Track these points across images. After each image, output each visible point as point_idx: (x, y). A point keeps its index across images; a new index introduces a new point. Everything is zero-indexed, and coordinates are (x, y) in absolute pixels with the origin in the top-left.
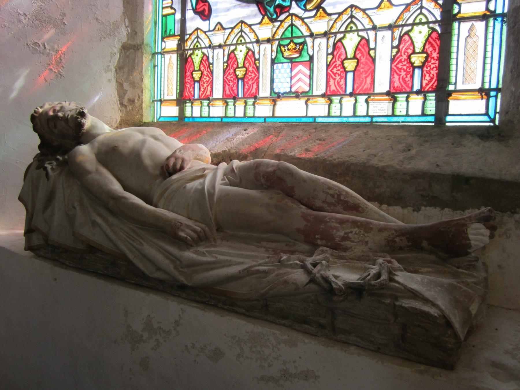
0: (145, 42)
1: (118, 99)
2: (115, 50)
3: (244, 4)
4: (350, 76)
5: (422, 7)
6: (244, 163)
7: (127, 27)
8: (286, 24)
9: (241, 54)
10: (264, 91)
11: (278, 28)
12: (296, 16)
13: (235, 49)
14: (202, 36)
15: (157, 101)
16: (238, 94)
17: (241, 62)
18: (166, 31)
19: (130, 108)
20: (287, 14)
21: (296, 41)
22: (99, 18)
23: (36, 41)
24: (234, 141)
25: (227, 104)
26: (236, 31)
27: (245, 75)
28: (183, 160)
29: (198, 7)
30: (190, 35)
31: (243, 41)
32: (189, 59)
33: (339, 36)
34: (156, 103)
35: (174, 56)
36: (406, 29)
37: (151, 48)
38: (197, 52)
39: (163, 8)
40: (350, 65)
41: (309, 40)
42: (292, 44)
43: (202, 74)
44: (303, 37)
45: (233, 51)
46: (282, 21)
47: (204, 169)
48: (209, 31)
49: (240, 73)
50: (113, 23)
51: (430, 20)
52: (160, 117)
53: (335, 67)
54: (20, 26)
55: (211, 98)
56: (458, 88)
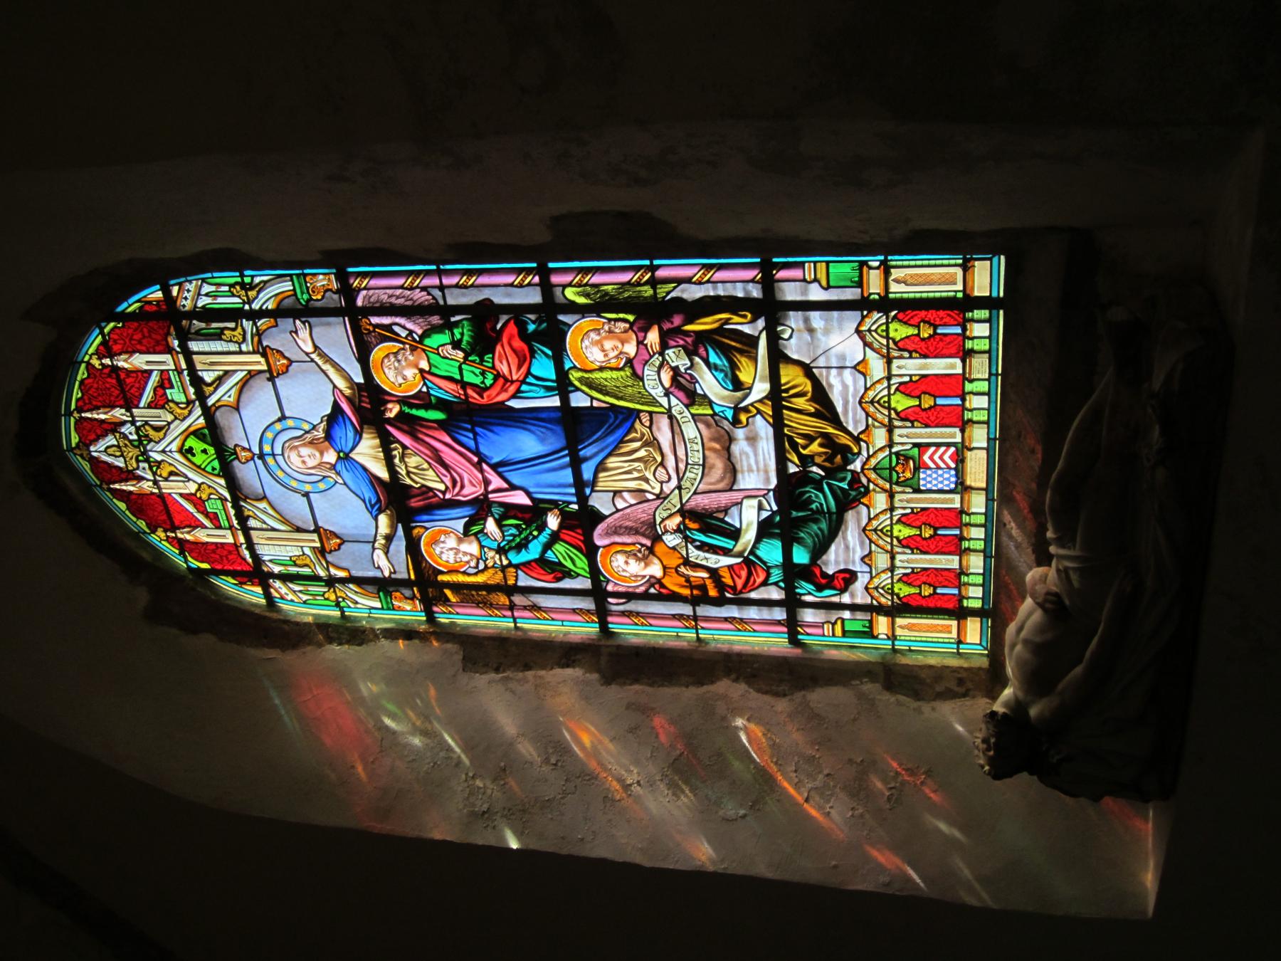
0: (879, 660)
1: (957, 700)
2: (893, 699)
3: (843, 527)
4: (940, 401)
5: (869, 331)
6: (1050, 526)
7: (862, 683)
8: (873, 476)
9: (903, 532)
10: (955, 502)
11: (877, 485)
12: (864, 464)
13: (897, 538)
14: (876, 581)
15: (958, 648)
16: (956, 535)
17: (914, 532)
18: (864, 632)
19: (970, 685)
20: (861, 475)
21: (894, 464)
22: (852, 716)
23: (886, 798)
24: (1019, 539)
25: (968, 550)
26: (874, 537)
27: (931, 526)
28: (1048, 593)
29: (838, 586)
30: (872, 598)
31: (889, 528)
32: (904, 600)
33: (893, 415)
34: (961, 651)
35: (899, 621)
36: (891, 345)
37: (886, 653)
38: (896, 590)
39: (834, 635)
40: (927, 402)
41: (894, 450)
42: (897, 469)
43: (925, 583)
44: (890, 455)
45: (899, 541)
46: (869, 481)
47: (1058, 571)
48: (871, 572)
49: (928, 533)
50: (858, 699)
51: (884, 321)
52: (980, 644)
53: (928, 418)
54: (867, 816)
55: (958, 571)
56: (961, 288)
